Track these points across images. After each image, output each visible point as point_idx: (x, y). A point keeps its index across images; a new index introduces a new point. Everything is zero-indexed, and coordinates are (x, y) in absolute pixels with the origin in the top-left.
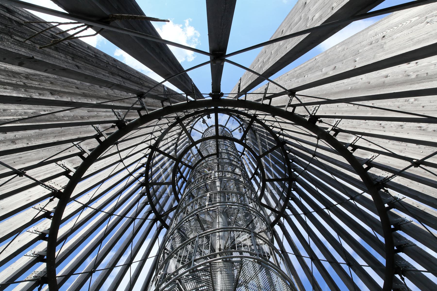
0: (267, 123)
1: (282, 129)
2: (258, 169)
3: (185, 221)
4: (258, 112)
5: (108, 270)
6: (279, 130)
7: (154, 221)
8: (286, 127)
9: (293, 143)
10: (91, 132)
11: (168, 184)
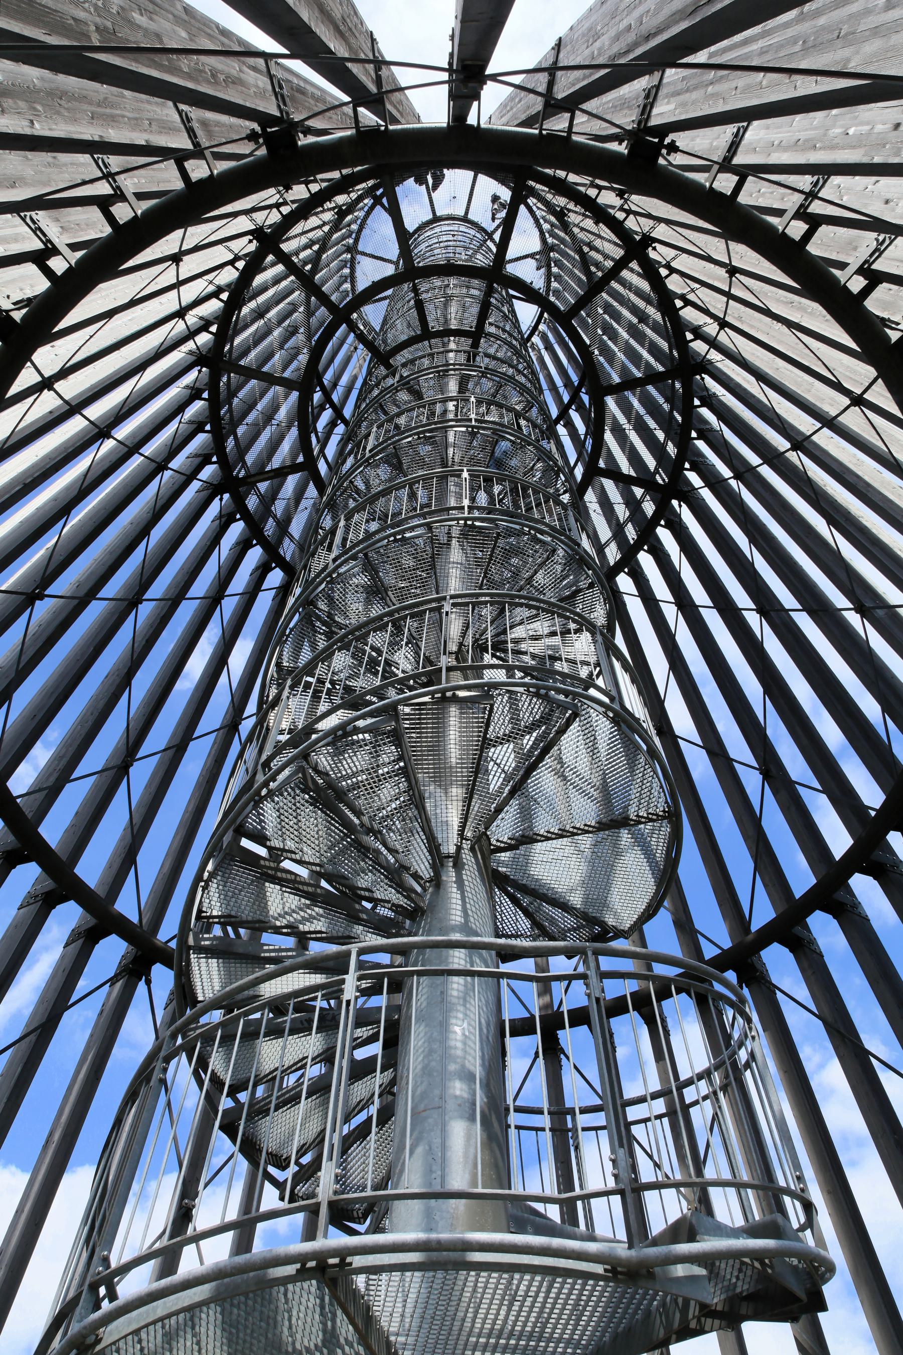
0: (674, 284)
1: (723, 324)
2: (583, 390)
3: (392, 539)
5: (76, 602)
7: (213, 490)
8: (740, 318)
9: (732, 380)
10: (166, 128)
11: (289, 384)
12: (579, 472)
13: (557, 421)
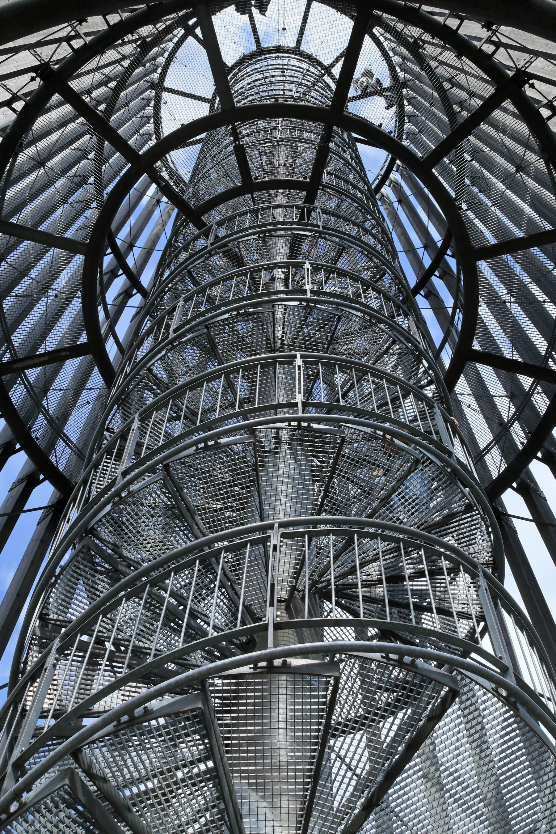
2: (449, 252)
4: (427, 37)
6: (464, 95)
12: (446, 357)
13: (416, 291)
